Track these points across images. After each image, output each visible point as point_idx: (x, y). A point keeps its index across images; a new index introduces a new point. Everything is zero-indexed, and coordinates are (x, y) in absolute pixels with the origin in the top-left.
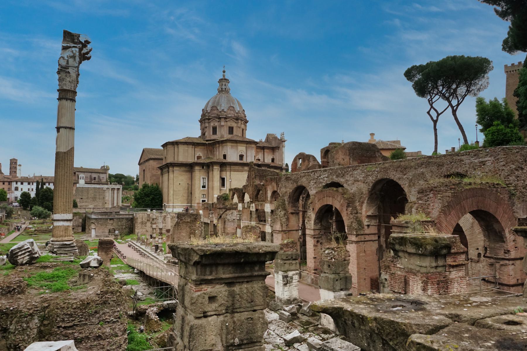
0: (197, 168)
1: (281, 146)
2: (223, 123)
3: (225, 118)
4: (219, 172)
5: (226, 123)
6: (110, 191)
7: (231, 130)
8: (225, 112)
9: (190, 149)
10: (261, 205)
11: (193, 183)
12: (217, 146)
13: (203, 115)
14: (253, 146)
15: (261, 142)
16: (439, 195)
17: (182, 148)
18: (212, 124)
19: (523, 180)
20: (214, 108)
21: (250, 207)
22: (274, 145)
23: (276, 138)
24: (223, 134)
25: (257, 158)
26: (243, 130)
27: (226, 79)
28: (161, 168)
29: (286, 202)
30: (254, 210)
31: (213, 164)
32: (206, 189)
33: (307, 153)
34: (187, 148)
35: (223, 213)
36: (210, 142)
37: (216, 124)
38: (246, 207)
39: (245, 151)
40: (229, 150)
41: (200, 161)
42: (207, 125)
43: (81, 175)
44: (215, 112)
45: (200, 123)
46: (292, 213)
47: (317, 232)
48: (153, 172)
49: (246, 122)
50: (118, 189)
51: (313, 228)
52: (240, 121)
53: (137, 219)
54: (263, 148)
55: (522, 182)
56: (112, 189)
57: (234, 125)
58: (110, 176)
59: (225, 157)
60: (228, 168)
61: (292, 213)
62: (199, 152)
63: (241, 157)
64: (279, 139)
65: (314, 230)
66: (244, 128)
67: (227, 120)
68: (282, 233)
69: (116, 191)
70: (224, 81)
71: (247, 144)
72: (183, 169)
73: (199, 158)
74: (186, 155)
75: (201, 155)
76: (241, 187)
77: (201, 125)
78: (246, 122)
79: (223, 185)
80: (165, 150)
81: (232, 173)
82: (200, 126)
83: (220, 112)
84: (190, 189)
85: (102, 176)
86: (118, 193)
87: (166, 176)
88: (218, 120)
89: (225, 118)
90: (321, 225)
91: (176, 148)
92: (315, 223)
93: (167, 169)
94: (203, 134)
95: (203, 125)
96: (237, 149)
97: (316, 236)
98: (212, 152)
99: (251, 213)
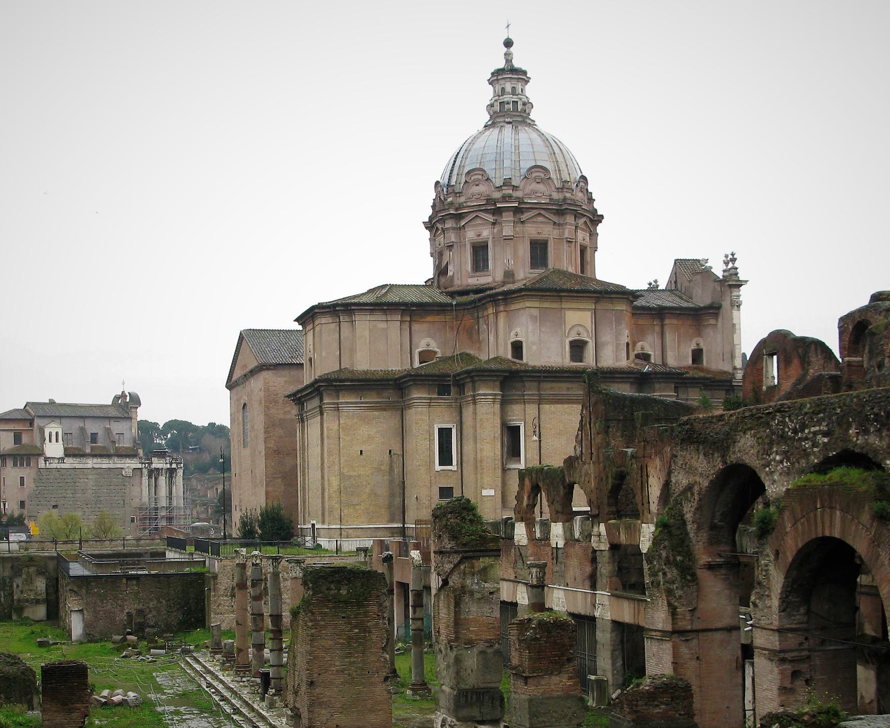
0: (417, 394)
1: (726, 304)
3: (517, 211)
4: (497, 406)
5: (519, 228)
6: (145, 479)
8: (515, 188)
9: (392, 328)
10: (628, 528)
11: (408, 447)
12: (491, 311)
13: (438, 206)
14: (622, 307)
15: (653, 289)
17: (364, 324)
18: (470, 235)
21: (590, 536)
22: (702, 298)
23: (707, 273)
24: (509, 263)
25: (638, 350)
27: (514, 71)
28: (299, 398)
29: (690, 527)
30: (605, 546)
32: (454, 467)
33: (798, 333)
34: (383, 325)
35: (452, 571)
36: (464, 299)
37: (486, 233)
38: (577, 535)
42: (452, 237)
43: (53, 428)
44: (483, 188)
45: (427, 233)
46: (710, 567)
47: (793, 640)
48: (273, 411)
49: (597, 219)
51: (776, 624)
52: (570, 219)
53: (215, 577)
54: (660, 313)
57: (545, 230)
58: (147, 428)
59: (517, 347)
60: (531, 390)
61: (710, 567)
62: (429, 339)
63: (578, 347)
64: (716, 279)
65: (780, 631)
66: (587, 242)
67: (524, 217)
68: (675, 638)
69: (163, 480)
70: (509, 75)
71: (597, 300)
72: (372, 398)
73: (425, 356)
74: (380, 349)
75: (434, 346)
76: (557, 462)
77: (432, 240)
78: (597, 219)
79: (513, 449)
80: (310, 335)
81: (546, 407)
82: (427, 244)
83: (499, 188)
84: (397, 471)
85: (117, 427)
86: (170, 484)
87: (313, 428)
88: (490, 218)
89: (517, 211)
90: (808, 612)
91: (345, 327)
92: (786, 606)
93: (315, 402)
94: (441, 271)
96: (562, 321)
97: (788, 656)
98: (473, 335)
99: (594, 560)
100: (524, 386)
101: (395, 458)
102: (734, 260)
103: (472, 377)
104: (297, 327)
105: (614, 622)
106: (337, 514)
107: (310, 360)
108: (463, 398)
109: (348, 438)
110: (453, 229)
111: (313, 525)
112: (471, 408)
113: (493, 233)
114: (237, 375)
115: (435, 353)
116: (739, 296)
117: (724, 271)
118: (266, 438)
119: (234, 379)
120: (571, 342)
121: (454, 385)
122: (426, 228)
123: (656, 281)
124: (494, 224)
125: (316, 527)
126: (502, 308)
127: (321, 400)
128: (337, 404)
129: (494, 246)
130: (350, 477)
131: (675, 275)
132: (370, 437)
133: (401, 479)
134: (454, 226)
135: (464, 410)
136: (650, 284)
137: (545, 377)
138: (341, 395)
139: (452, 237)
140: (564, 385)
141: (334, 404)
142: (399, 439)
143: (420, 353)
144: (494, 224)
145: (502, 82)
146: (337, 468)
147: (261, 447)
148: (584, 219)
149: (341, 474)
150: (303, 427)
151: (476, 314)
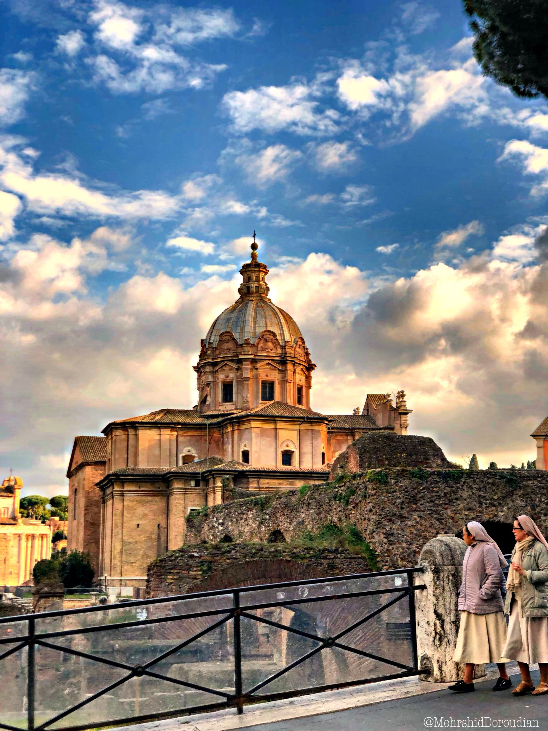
0: (177, 485)
2: (247, 374)
7: (268, 391)
12: (230, 429)
16: (171, 577)
18: (221, 377)
19: (407, 542)
20: (226, 337)
26: (300, 390)
27: (258, 265)
31: (213, 474)
36: (215, 421)
39: (297, 442)
40: (254, 440)
41: (190, 469)
45: (196, 374)
50: (42, 536)
55: (405, 545)
56: (28, 536)
59: (246, 456)
63: (287, 457)
73: (187, 459)
75: (194, 453)
77: (199, 379)
84: (163, 539)
88: (235, 366)
94: (203, 401)
95: (203, 378)
98: (220, 445)
100: (249, 481)
101: (162, 529)
102: (403, 396)
103: (213, 475)
104: (102, 435)
105: (497, 664)
106: (118, 569)
107: (109, 460)
108: (208, 489)
109: (129, 516)
110: (210, 372)
111: (106, 577)
112: (111, 501)
113: (237, 376)
114: (74, 467)
115: (194, 457)
116: (406, 420)
117: (397, 403)
118: (85, 514)
119: (72, 470)
120: (283, 452)
121: (202, 480)
122: (195, 371)
123: (358, 409)
124: (237, 370)
125: (107, 579)
126: (236, 428)
127: (113, 488)
128: (123, 491)
129: (237, 385)
130: (130, 543)
131: (367, 404)
132: (145, 515)
133: (165, 545)
134: (211, 370)
135: (208, 497)
136: (354, 411)
137: (262, 475)
138: (125, 485)
139: (210, 379)
140: (276, 481)
141: (121, 491)
142: (165, 516)
143: (184, 457)
144: (237, 370)
145: (249, 273)
146: (120, 536)
147: (82, 520)
148: (301, 367)
149: (122, 541)
150: (104, 507)
151: (221, 431)
